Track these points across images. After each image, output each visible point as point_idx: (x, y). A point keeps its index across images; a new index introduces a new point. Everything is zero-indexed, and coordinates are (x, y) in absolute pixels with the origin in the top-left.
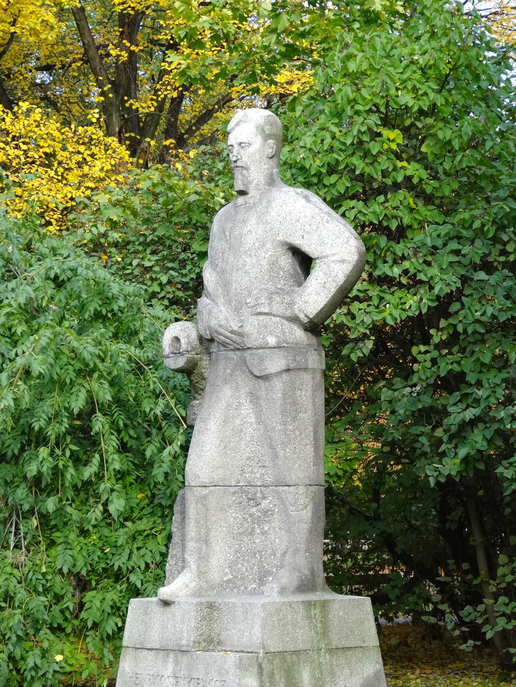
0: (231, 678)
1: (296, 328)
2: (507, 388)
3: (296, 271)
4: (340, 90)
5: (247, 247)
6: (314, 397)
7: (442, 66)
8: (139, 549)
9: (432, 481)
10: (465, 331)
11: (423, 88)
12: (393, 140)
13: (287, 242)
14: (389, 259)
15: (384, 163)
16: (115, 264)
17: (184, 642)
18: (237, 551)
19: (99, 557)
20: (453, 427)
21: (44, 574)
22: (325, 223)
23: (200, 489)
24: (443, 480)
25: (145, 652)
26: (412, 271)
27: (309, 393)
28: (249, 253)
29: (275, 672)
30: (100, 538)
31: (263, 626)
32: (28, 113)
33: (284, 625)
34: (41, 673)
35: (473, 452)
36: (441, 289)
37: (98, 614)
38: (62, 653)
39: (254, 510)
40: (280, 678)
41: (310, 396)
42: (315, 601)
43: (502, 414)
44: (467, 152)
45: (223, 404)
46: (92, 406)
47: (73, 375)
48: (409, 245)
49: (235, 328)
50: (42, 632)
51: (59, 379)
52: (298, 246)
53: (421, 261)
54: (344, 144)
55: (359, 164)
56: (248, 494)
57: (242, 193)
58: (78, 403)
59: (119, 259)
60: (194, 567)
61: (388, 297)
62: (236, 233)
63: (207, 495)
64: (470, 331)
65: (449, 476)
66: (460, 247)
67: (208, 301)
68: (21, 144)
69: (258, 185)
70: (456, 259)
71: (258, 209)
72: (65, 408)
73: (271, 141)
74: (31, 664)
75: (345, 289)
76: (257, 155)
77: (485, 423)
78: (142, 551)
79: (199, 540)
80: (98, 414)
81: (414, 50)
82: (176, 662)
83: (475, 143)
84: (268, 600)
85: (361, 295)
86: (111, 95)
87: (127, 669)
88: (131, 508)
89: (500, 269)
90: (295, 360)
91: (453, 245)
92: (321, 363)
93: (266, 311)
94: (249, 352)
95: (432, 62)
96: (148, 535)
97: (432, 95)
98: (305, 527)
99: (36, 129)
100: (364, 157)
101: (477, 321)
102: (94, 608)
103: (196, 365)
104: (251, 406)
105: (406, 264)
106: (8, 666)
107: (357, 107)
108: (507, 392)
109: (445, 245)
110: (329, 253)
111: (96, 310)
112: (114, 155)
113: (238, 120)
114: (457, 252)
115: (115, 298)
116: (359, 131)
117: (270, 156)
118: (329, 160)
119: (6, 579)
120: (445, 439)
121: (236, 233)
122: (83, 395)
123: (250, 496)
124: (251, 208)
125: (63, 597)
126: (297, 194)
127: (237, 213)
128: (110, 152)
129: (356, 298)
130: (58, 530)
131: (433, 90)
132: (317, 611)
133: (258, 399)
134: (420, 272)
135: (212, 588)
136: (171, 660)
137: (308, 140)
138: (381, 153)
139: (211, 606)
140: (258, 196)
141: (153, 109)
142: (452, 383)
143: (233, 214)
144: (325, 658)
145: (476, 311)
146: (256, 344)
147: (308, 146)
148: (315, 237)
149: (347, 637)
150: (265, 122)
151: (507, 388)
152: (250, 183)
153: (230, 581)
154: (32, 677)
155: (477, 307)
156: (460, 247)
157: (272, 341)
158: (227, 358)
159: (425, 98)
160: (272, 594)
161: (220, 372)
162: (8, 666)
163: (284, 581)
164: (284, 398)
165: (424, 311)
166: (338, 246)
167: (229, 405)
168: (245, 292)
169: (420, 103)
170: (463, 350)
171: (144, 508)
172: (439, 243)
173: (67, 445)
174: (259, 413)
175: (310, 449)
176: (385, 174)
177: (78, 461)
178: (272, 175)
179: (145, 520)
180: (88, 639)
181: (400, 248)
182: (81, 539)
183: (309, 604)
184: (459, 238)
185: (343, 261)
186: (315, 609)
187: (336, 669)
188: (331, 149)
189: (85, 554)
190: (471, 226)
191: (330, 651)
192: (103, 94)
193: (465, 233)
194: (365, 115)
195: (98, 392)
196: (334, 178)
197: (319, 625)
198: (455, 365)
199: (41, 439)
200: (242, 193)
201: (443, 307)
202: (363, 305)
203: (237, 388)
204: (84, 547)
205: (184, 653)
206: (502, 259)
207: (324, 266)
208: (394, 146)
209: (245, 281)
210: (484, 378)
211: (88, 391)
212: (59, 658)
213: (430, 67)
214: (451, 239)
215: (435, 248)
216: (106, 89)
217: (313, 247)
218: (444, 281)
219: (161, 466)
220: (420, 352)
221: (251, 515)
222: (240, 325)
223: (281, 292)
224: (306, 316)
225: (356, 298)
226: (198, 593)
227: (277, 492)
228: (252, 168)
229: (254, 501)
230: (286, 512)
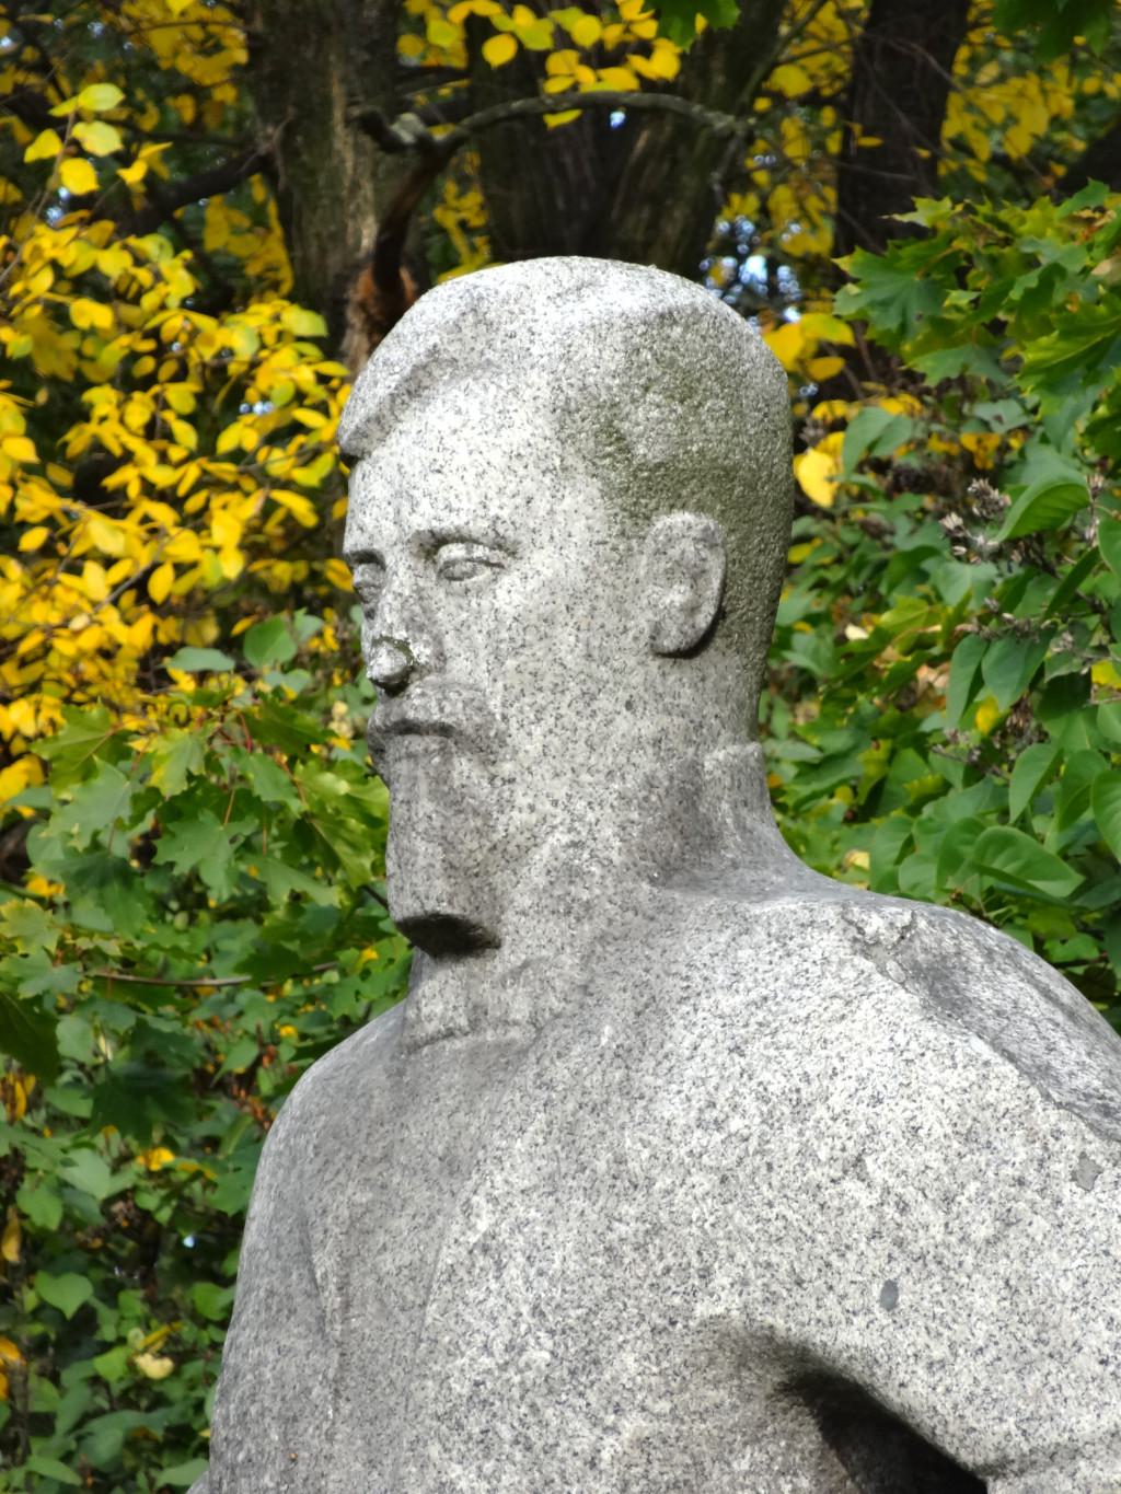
5: (467, 1367)
13: (770, 1336)
16: (126, 1401)
22: (1067, 1190)
52: (858, 1372)
57: (452, 939)
59: (155, 1367)
62: (388, 1263)
69: (573, 874)
71: (560, 1072)
73: (681, 518)
76: (566, 639)
112: (279, 462)
113: (420, 348)
117: (669, 644)
121: (388, 1263)
124: (510, 1057)
126: (866, 946)
127: (406, 1094)
128: (239, 435)
140: (568, 960)
143: (381, 1101)
148: (985, 1299)
150: (632, 365)
152: (512, 855)
178: (690, 790)
217: (967, 1373)
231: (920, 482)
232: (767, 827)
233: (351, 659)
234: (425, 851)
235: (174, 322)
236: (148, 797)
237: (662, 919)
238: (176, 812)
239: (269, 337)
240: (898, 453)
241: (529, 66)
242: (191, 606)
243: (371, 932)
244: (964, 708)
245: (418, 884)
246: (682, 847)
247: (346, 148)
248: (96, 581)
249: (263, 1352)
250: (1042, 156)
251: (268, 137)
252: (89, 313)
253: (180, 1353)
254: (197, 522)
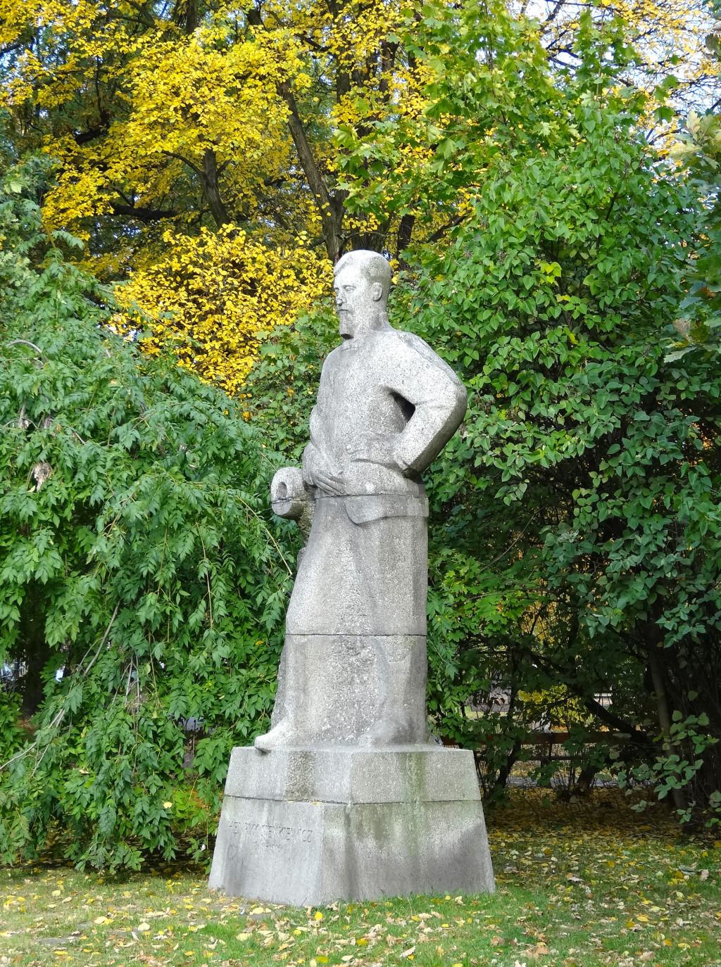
1: (395, 475)
2: (670, 534)
3: (399, 417)
4: (495, 221)
5: (349, 392)
6: (414, 544)
7: (602, 195)
8: (250, 696)
9: (592, 632)
10: (624, 474)
11: (581, 219)
12: (551, 274)
14: (545, 398)
15: (540, 297)
17: (278, 791)
18: (336, 701)
19: (213, 704)
20: (615, 575)
21: (155, 721)
24: (602, 631)
25: (244, 801)
26: (569, 411)
27: (409, 541)
29: (364, 823)
30: (215, 685)
31: (353, 777)
32: (231, 236)
33: (376, 776)
34: (148, 820)
35: (632, 602)
36: (597, 430)
37: (211, 761)
38: (171, 800)
39: (353, 659)
40: (369, 830)
41: (410, 543)
42: (411, 753)
43: (663, 562)
44: (628, 285)
45: (323, 551)
46: (198, 552)
47: (181, 520)
48: (566, 384)
49: (335, 475)
50: (150, 778)
51: (167, 524)
53: (578, 401)
54: (497, 278)
55: (511, 299)
56: (348, 643)
57: (347, 337)
58: (184, 548)
60: (291, 715)
61: (544, 438)
64: (629, 474)
65: (609, 626)
66: (621, 386)
68: (220, 270)
70: (615, 398)
72: (173, 553)
74: (139, 810)
75: (444, 435)
77: (648, 571)
78: (254, 699)
79: (297, 689)
80: (206, 560)
81: (574, 178)
82: (270, 812)
83: (638, 275)
84: (359, 750)
85: (515, 436)
86: (329, 214)
87: (228, 817)
88: (248, 655)
89: (670, 408)
90: (393, 507)
91: (614, 384)
92: (423, 511)
94: (349, 499)
95: (591, 191)
96: (261, 683)
97: (590, 226)
98: (403, 677)
99: (239, 253)
100: (517, 293)
101: (637, 464)
102: (207, 756)
103: (302, 511)
104: (352, 554)
105: (563, 404)
106: (117, 812)
107: (512, 240)
108: (670, 538)
109: (606, 383)
110: (427, 398)
111: (214, 454)
112: (327, 279)
114: (617, 391)
115: (232, 441)
116: (511, 266)
118: (481, 295)
119: (118, 725)
120: (608, 587)
122: (190, 541)
123: (349, 645)
124: (355, 352)
125: (175, 744)
126: (400, 338)
127: (342, 356)
128: (322, 276)
129: (510, 440)
130: (175, 677)
131: (593, 221)
132: (413, 763)
133: (358, 546)
134: (576, 411)
135: (310, 738)
136: (265, 809)
137: (462, 274)
138: (537, 288)
139: (306, 755)
141: (375, 228)
142: (614, 527)
144: (420, 811)
145: (637, 453)
146: (355, 491)
147: (462, 281)
148: (415, 382)
149: (445, 791)
151: (670, 534)
152: (355, 326)
153: (328, 730)
154: (140, 824)
155: (639, 449)
156: (621, 386)
157: (370, 488)
158: (328, 505)
159: (584, 229)
160: (366, 745)
162: (117, 812)
163: (380, 732)
164: (382, 546)
165: (581, 453)
166: (437, 389)
167: (329, 553)
169: (578, 234)
170: (625, 495)
171: (261, 655)
172: (598, 381)
173: (178, 591)
174: (358, 561)
175: (409, 598)
176: (542, 309)
177: (189, 606)
179: (261, 667)
180: (200, 787)
181: (555, 388)
182: (197, 686)
183: (404, 756)
184: (621, 377)
185: (441, 407)
186: (410, 761)
187: (432, 822)
188: (484, 284)
189: (199, 700)
190: (633, 364)
191: (425, 804)
192: (322, 213)
193: (626, 371)
194: (520, 248)
195: (206, 538)
196: (485, 314)
197: (414, 777)
198: (615, 509)
199: (149, 584)
200: (347, 337)
201: (601, 448)
202: (518, 447)
203: (337, 535)
204: (199, 694)
206: (673, 397)
208: (551, 280)
209: (347, 427)
210: (645, 524)
211: (196, 538)
212: (168, 805)
213: (590, 197)
214: (613, 377)
215: (595, 386)
216: (323, 207)
217: (412, 392)
218: (600, 420)
219: (270, 613)
220: (581, 496)
223: (381, 438)
224: (405, 463)
225: (510, 440)
226: (295, 742)
227: (377, 642)
228: (357, 312)
230: (384, 661)
231: (408, 281)
232: (388, 323)
233: (335, 303)
234: (344, 326)
235: (314, 261)
236: (310, 319)
237: (374, 334)
238: (314, 321)
239: (325, 263)
240: (405, 277)
241: (358, 229)
242: (316, 298)
243: (339, 336)
244: (413, 308)
245: (343, 331)
246: (377, 325)
247: (335, 239)
248: (304, 294)
249: (323, 388)
250: (424, 239)
251: (325, 238)
252: (303, 260)
253: (314, 391)
254: (317, 287)
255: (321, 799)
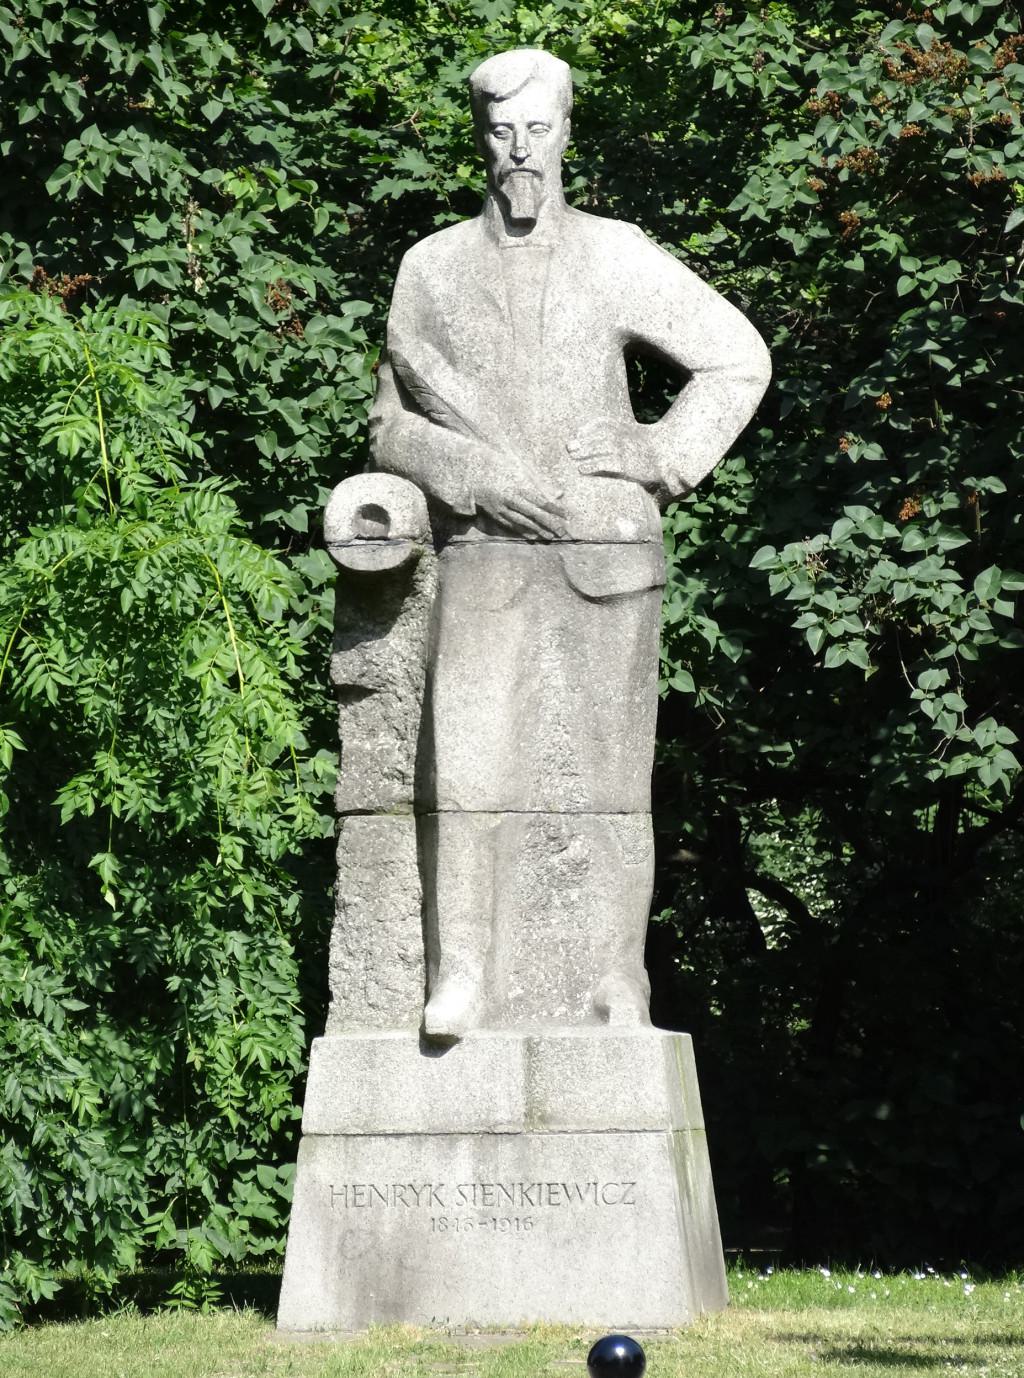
0: (652, 1175)
23: (485, 816)
25: (380, 1142)
28: (566, 349)
39: (555, 860)
49: (552, 500)
62: (522, 305)
63: (498, 828)
67: (459, 437)
71: (567, 260)
93: (616, 469)
146: (594, 533)
153: (519, 999)
161: (497, 582)
168: (563, 429)
174: (575, 670)
185: (751, 380)
203: (534, 618)
205: (422, 1138)
207: (716, 386)
217: (691, 347)
221: (549, 870)
222: (559, 493)
229: (558, 842)
255: (573, 1127)
